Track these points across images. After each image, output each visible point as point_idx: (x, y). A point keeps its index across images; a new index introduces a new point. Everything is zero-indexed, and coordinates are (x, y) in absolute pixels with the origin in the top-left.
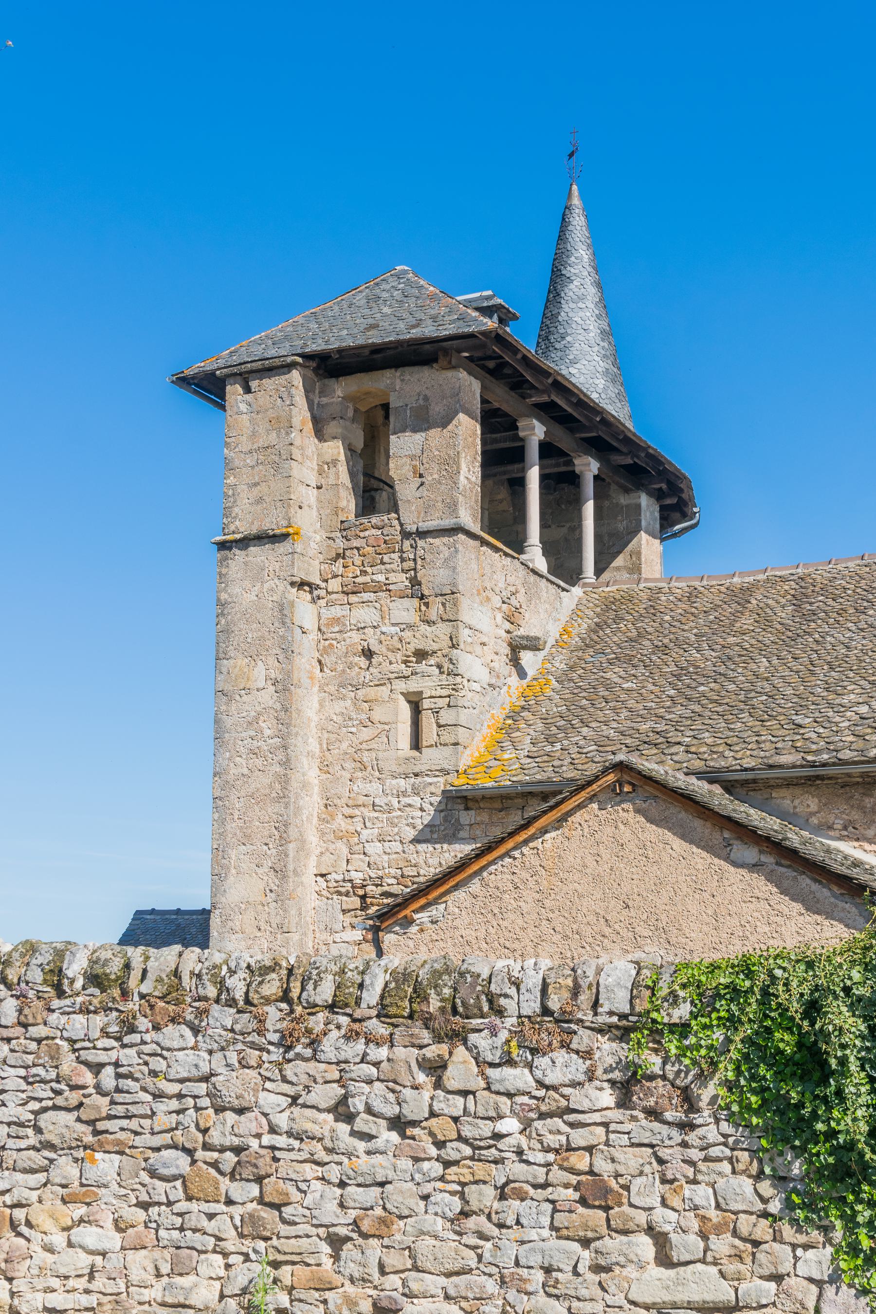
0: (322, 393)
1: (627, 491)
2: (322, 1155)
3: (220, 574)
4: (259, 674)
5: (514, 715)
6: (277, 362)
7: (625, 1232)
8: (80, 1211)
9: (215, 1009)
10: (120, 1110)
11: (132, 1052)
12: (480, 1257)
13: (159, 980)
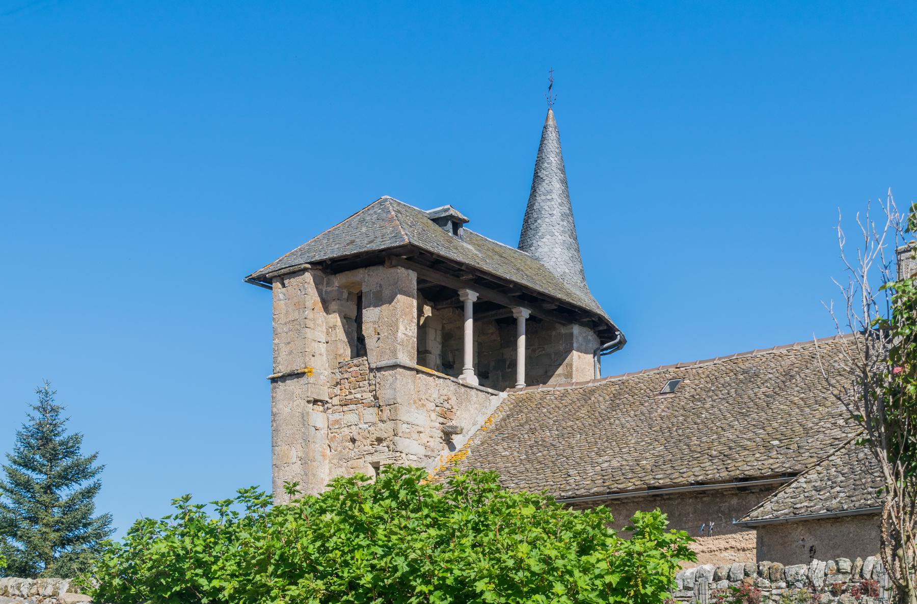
0: (328, 285)
3: (272, 397)
4: (294, 454)
6: (296, 268)
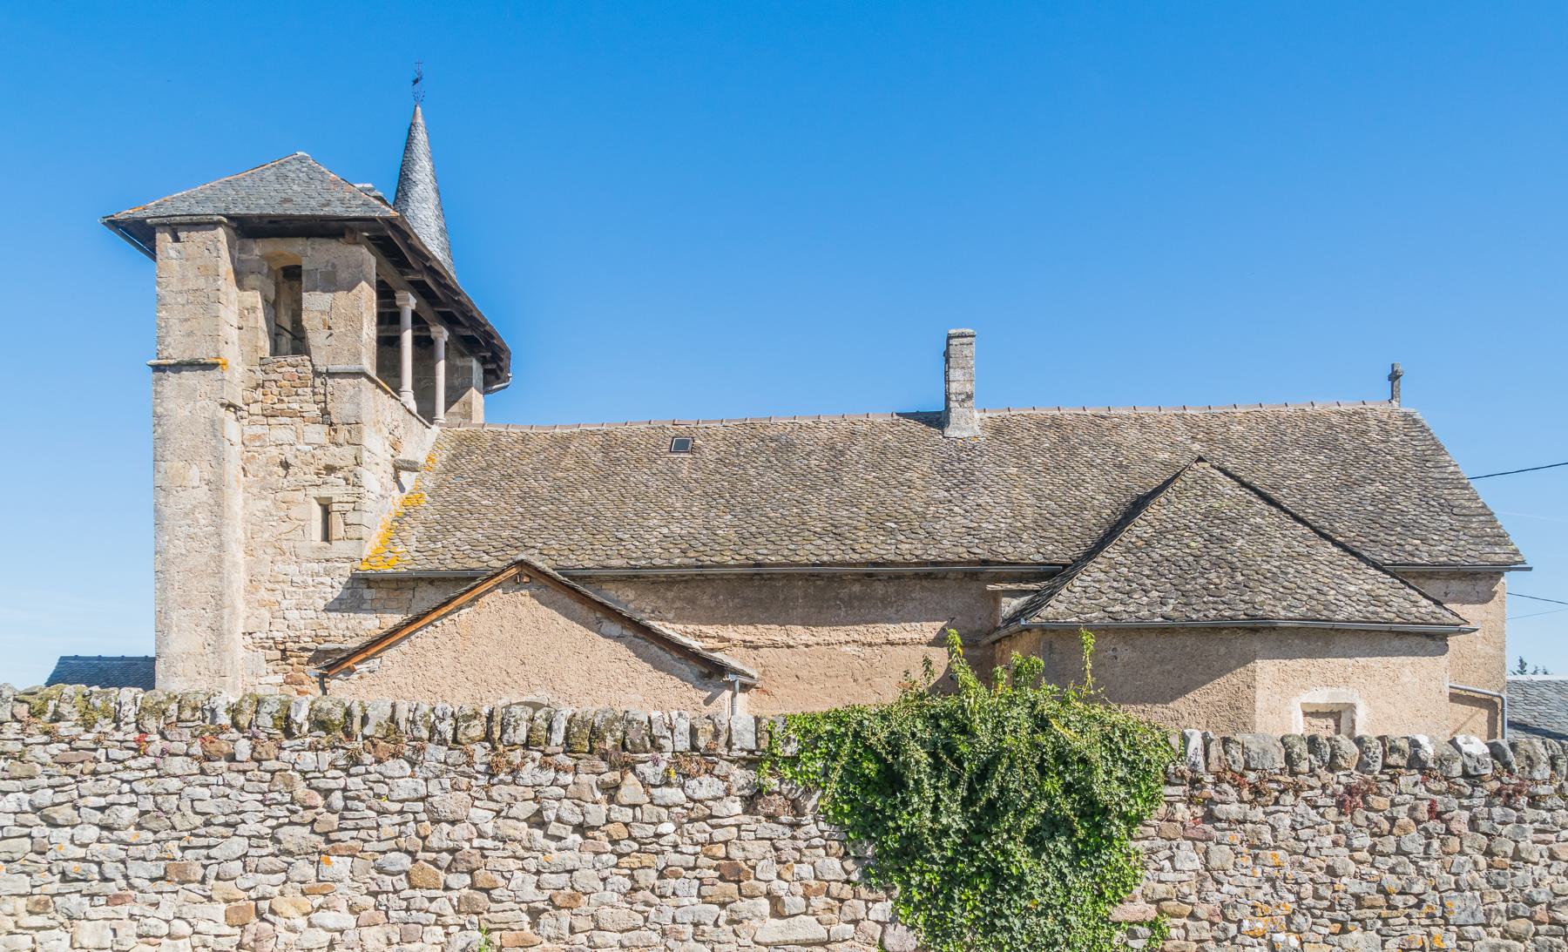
0: (241, 250)
1: (462, 355)
2: (521, 852)
4: (194, 474)
5: (399, 519)
6: (205, 219)
7: (752, 897)
8: (320, 900)
9: (430, 747)
10: (350, 824)
11: (358, 780)
12: (646, 919)
13: (379, 725)
